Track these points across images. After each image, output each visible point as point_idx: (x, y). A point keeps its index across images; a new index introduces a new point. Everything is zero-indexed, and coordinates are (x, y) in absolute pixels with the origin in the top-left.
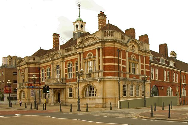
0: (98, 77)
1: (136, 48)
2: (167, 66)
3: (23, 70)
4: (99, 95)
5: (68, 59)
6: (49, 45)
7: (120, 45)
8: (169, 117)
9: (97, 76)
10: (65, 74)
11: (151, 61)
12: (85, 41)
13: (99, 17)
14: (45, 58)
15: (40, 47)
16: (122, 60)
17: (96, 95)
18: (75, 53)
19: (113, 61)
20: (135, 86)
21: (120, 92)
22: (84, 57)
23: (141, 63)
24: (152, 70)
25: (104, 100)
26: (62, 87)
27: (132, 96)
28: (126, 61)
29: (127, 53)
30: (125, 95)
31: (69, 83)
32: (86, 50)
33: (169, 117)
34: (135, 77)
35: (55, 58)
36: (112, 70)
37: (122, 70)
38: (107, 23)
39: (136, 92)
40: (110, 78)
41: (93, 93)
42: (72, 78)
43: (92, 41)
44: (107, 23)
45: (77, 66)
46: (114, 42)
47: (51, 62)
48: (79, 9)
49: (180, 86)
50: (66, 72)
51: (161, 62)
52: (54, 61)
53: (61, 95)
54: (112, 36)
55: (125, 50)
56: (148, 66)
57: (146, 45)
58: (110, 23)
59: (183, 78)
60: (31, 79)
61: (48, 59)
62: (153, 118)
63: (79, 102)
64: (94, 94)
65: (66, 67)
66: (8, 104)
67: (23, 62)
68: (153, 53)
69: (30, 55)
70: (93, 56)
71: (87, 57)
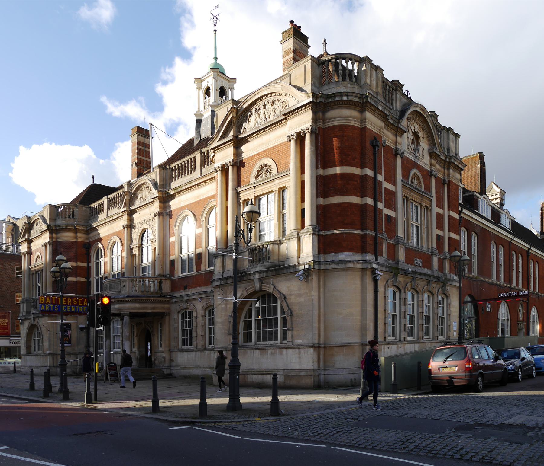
4: (304, 335)
15: (93, 178)
17: (289, 334)
19: (362, 186)
25: (322, 357)
26: (159, 307)
37: (384, 229)
42: (194, 272)
48: (215, 31)
53: (156, 338)
55: (393, 146)
56: (455, 219)
64: (279, 329)
66: (300, 353)
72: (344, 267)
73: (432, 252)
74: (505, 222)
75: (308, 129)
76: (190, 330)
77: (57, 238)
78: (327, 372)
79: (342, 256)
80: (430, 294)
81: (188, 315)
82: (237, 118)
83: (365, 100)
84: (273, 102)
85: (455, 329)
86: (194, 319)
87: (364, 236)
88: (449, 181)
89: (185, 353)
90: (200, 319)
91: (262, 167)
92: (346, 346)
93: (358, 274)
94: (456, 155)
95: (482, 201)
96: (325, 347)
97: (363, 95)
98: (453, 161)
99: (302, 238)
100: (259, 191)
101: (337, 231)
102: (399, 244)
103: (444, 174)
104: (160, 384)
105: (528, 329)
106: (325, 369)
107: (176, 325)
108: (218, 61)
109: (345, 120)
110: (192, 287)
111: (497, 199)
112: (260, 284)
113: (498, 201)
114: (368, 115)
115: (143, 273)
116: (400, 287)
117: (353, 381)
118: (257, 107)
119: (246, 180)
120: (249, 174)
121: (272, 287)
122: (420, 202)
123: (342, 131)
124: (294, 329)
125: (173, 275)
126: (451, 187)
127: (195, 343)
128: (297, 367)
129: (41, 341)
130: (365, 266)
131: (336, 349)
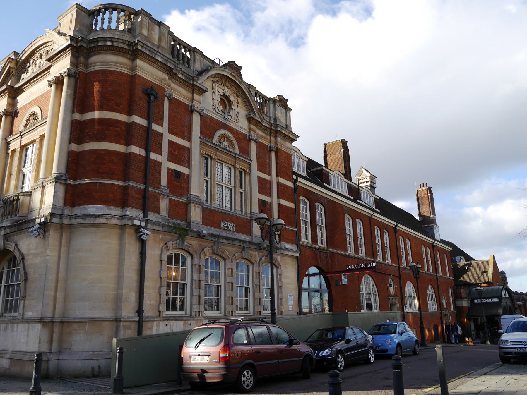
16: (171, 143)
19: (126, 134)
20: (229, 266)
28: (189, 150)
29: (196, 119)
34: (231, 226)
55: (188, 103)
72: (94, 223)
73: (251, 217)
74: (368, 199)
75: (65, 72)
78: (61, 357)
79: (92, 209)
80: (249, 263)
82: (16, 70)
83: (135, 48)
84: (48, 52)
85: (291, 303)
87: (125, 189)
88: (277, 148)
91: (31, 116)
92: (88, 322)
93: (115, 232)
94: (286, 126)
95: (334, 176)
96: (62, 322)
97: (132, 43)
98: (279, 129)
99: (46, 187)
100: (25, 141)
101: (88, 181)
102: (191, 203)
103: (271, 141)
105: (403, 303)
106: (60, 353)
109: (109, 65)
111: (367, 182)
112: (4, 242)
113: (369, 183)
114: (139, 62)
116: (191, 251)
117: (96, 369)
118: (35, 58)
119: (17, 129)
120: (19, 124)
121: (14, 245)
122: (233, 164)
123: (104, 76)
124: (27, 298)
126: (279, 154)
128: (24, 349)
130: (124, 222)
131: (75, 326)
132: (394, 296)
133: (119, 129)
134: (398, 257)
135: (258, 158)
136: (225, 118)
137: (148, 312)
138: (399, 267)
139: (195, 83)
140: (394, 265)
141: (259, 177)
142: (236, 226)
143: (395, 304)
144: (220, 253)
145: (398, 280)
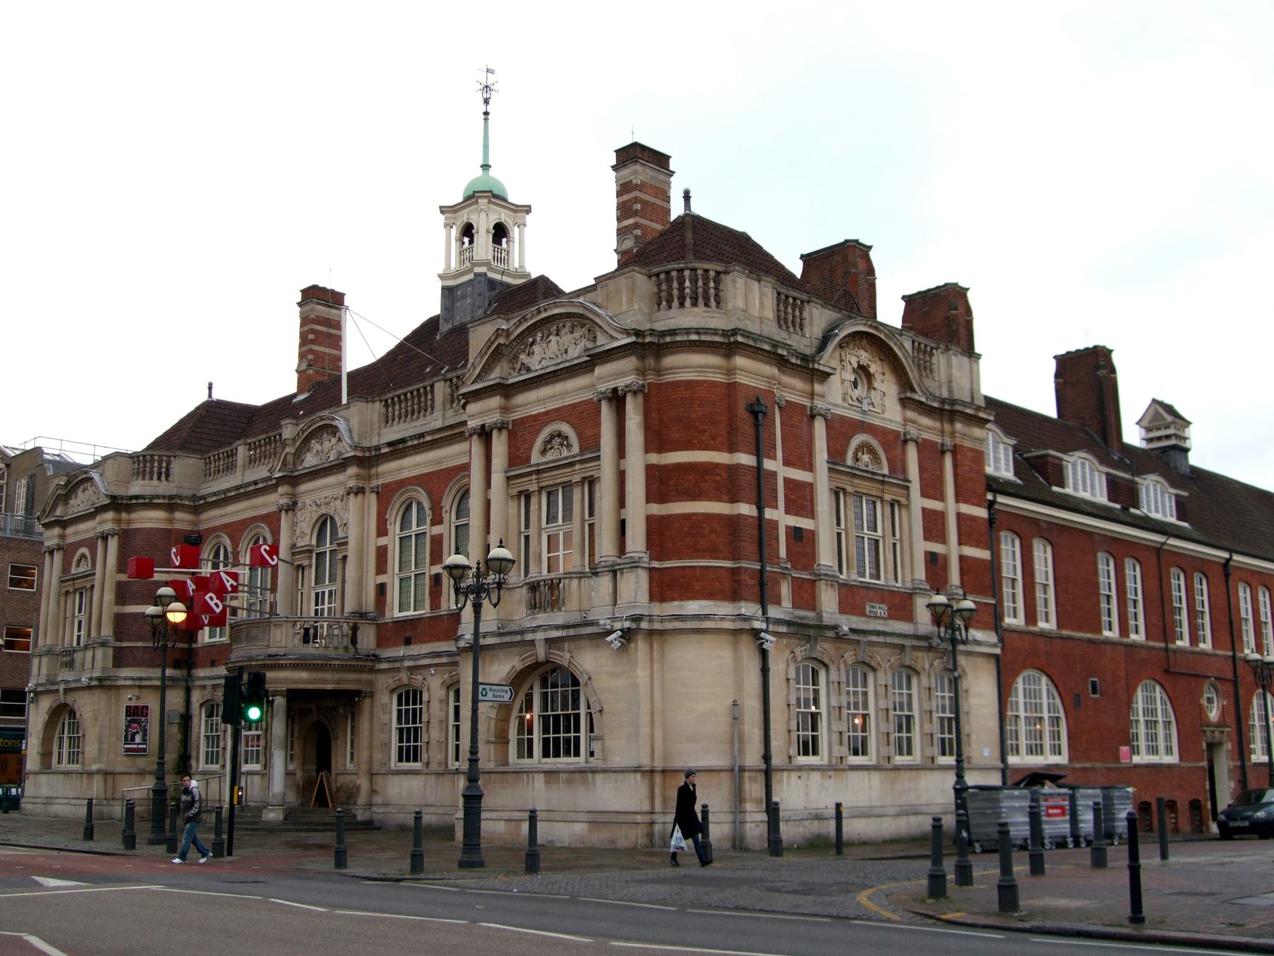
0: (615, 604)
1: (886, 386)
2: (1122, 517)
3: (84, 550)
5: (400, 469)
6: (265, 373)
7: (771, 370)
8: (1137, 915)
9: (608, 599)
10: (372, 581)
11: (996, 486)
12: (524, 340)
13: (625, 172)
14: (240, 463)
15: (210, 388)
16: (786, 480)
18: (451, 427)
19: (727, 483)
20: (882, 681)
21: (773, 726)
22: (517, 458)
23: (924, 495)
24: (1010, 550)
25: (657, 790)
26: (349, 681)
27: (859, 760)
28: (811, 486)
29: (820, 428)
30: (809, 747)
31: (401, 651)
32: (532, 402)
33: (1137, 915)
34: (881, 610)
35: (310, 460)
36: (714, 553)
37: (783, 552)
38: (677, 210)
39: (892, 727)
40: (697, 617)
41: (577, 730)
42: (425, 611)
43: (571, 346)
44: (677, 210)
45: (462, 521)
46: (728, 344)
47: (280, 490)
48: (486, 113)
49: (1230, 675)
50: (381, 567)
51: (1075, 489)
52: (303, 487)
54: (713, 303)
55: (806, 402)
56: (973, 519)
57: (958, 361)
58: (698, 209)
59: (1256, 612)
60: (143, 615)
61: (261, 472)
62: (1013, 924)
63: (473, 802)
64: (582, 735)
65: (382, 531)
67: (91, 490)
68: (1011, 418)
69: (138, 442)
70: (576, 449)
71: (534, 461)
76: (416, 729)
77: (129, 522)
81: (410, 696)
86: (424, 706)
87: (734, 571)
88: (955, 446)
89: (403, 777)
90: (435, 705)
104: (349, 839)
107: (385, 718)
108: (492, 172)
110: (422, 642)
115: (317, 604)
125: (383, 614)
126: (959, 457)
127: (425, 756)
129: (76, 741)
132: (1218, 725)
133: (718, 478)
134: (1231, 632)
135: (922, 469)
136: (864, 412)
137: (776, 760)
138: (1234, 657)
139: (816, 366)
140: (1219, 652)
141: (923, 509)
142: (889, 609)
143: (1220, 744)
144: (867, 660)
145: (1230, 687)
